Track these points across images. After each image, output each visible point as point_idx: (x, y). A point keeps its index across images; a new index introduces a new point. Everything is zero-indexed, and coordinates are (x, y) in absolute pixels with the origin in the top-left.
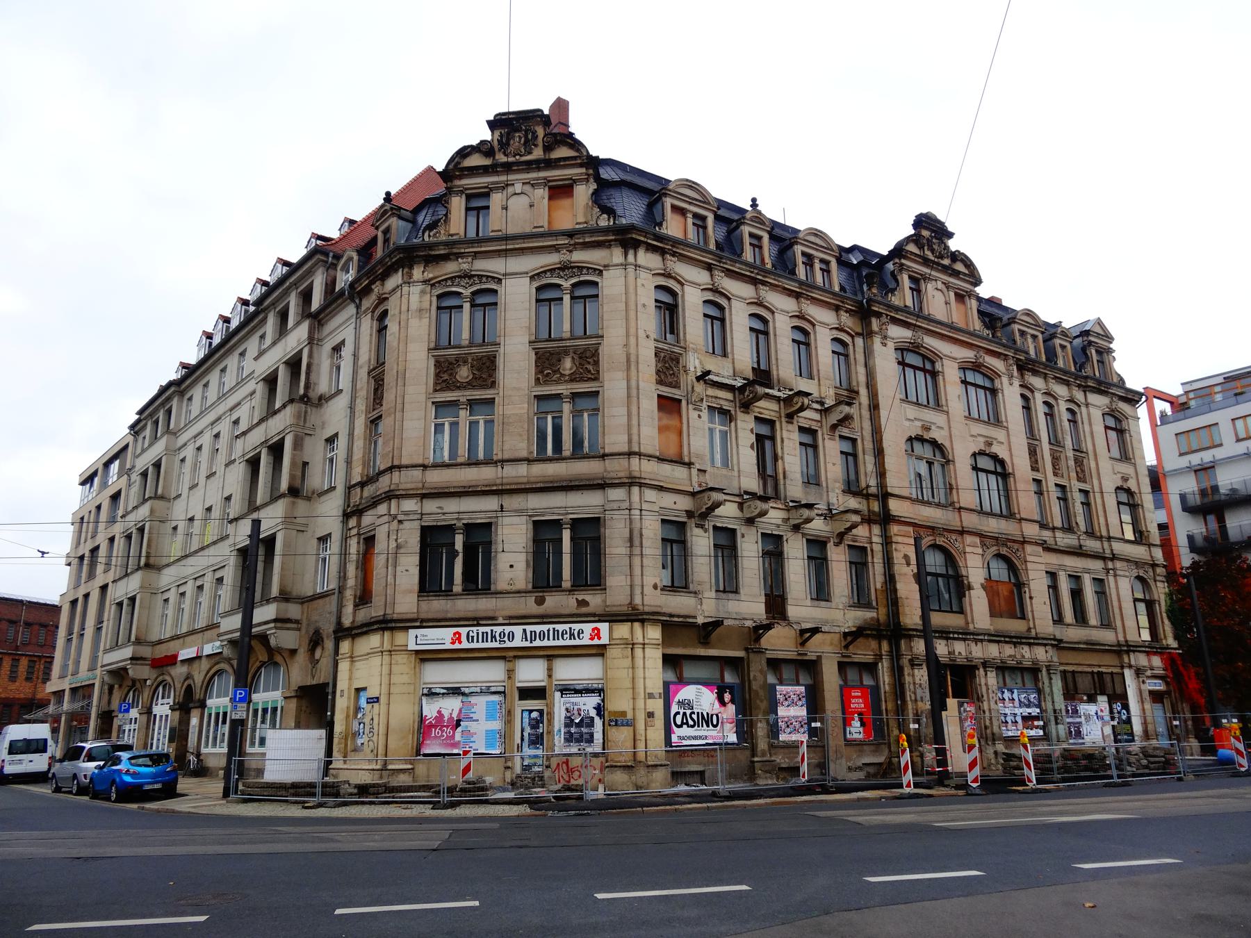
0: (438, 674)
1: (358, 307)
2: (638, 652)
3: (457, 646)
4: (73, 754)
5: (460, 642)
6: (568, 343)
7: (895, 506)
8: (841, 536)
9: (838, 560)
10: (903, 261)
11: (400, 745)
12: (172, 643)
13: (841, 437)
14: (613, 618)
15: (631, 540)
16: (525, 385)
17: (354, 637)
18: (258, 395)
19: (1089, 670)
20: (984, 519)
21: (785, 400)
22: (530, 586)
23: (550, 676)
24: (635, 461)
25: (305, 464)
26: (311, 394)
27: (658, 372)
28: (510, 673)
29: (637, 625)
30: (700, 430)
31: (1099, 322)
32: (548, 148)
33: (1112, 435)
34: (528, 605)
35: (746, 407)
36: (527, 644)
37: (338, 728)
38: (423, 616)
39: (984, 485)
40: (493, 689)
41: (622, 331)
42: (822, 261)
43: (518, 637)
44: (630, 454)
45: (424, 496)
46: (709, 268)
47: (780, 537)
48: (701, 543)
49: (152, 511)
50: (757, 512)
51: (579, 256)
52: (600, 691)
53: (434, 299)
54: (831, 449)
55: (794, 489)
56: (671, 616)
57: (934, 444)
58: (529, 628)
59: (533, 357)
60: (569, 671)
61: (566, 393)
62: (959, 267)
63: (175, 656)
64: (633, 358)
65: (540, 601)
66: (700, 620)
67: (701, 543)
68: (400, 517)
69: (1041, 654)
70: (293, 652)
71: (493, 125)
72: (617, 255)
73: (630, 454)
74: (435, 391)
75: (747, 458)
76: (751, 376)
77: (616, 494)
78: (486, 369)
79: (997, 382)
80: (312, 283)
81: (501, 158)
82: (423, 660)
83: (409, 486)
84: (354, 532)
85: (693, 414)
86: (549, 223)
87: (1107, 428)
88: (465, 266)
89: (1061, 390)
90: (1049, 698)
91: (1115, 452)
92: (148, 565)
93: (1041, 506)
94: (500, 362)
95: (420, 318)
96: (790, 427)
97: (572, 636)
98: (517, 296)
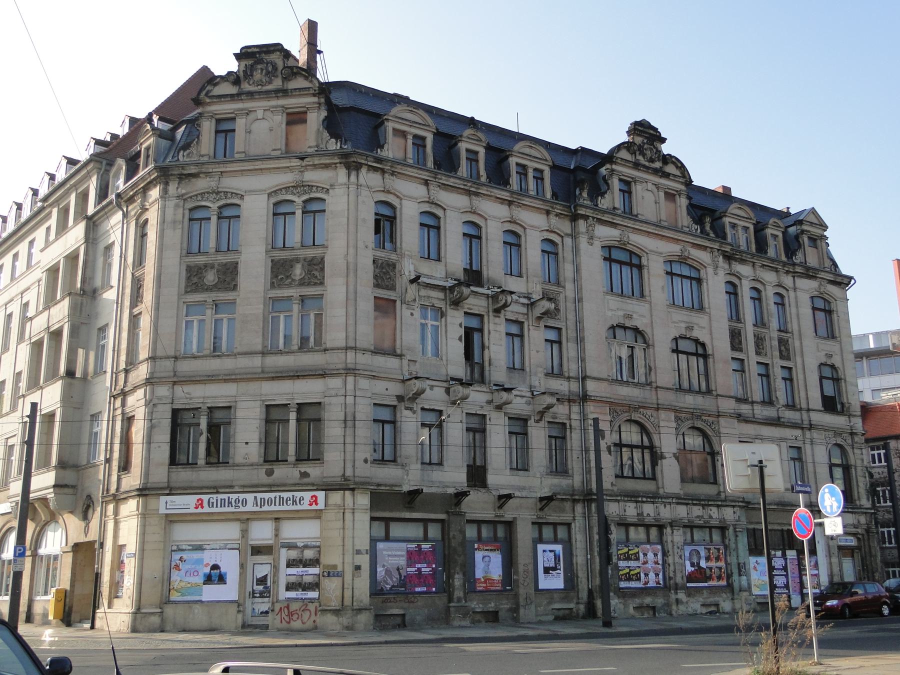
2: (348, 516)
3: (200, 510)
5: (202, 507)
7: (591, 386)
8: (542, 414)
9: (538, 435)
10: (614, 167)
13: (546, 326)
14: (328, 488)
16: (261, 288)
18: (43, 283)
19: (780, 528)
20: (680, 395)
21: (492, 297)
22: (262, 459)
23: (276, 535)
27: (375, 277)
28: (245, 533)
29: (347, 493)
30: (410, 325)
31: (813, 211)
32: (286, 79)
33: (821, 315)
35: (456, 304)
36: (258, 509)
39: (684, 366)
40: (229, 546)
41: (344, 243)
42: (535, 170)
43: (250, 502)
46: (426, 183)
47: (484, 416)
50: (460, 395)
51: (311, 176)
53: (187, 212)
54: (536, 336)
55: (498, 374)
56: (379, 485)
57: (636, 330)
58: (259, 496)
59: (270, 264)
60: (294, 531)
62: (670, 169)
64: (351, 267)
65: (270, 473)
66: (406, 488)
69: (729, 514)
71: (238, 57)
74: (186, 292)
75: (455, 349)
76: (461, 275)
77: (335, 383)
78: (229, 276)
79: (702, 272)
80: (89, 186)
81: (246, 87)
83: (163, 375)
85: (406, 313)
86: (287, 145)
87: (814, 309)
89: (770, 277)
90: (734, 553)
91: (822, 331)
93: (744, 384)
94: (241, 269)
95: (174, 229)
96: (497, 320)
97: (294, 502)
98: (255, 211)
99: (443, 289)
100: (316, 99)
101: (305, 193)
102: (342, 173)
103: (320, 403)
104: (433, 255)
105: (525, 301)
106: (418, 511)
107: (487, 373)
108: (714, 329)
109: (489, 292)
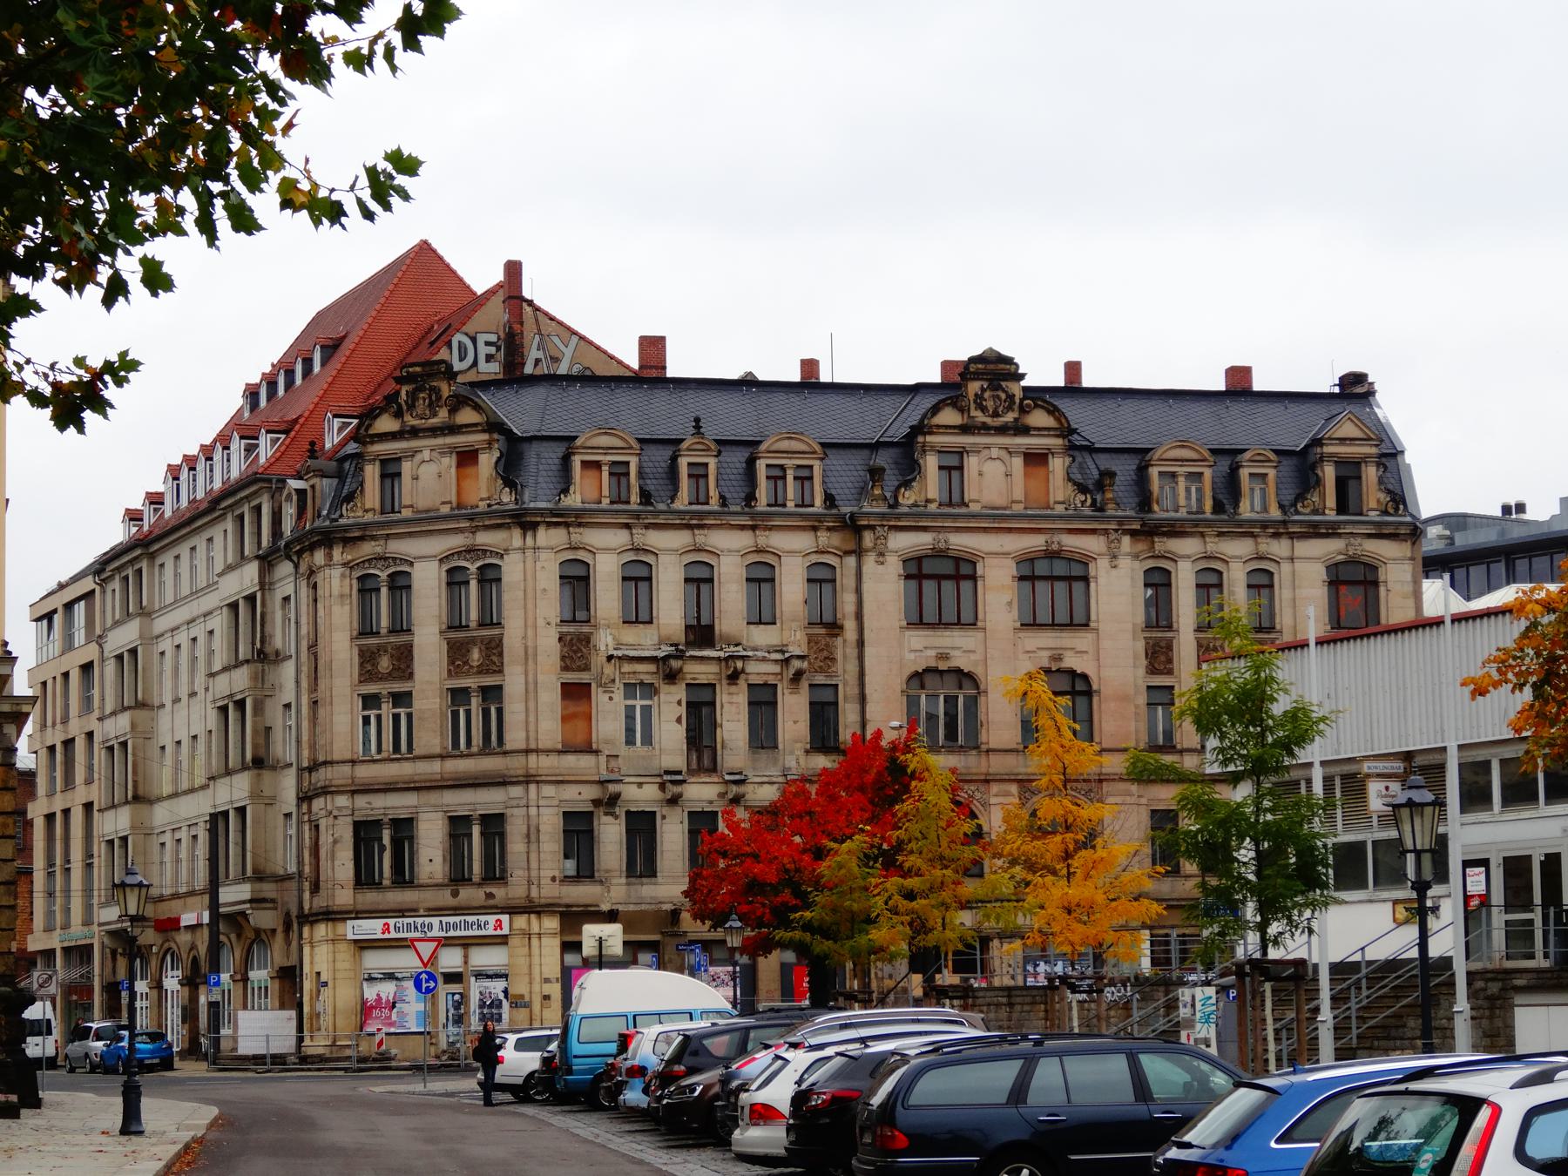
0: (376, 961)
1: (296, 566)
2: (535, 941)
3: (387, 936)
4: (78, 1033)
6: (475, 634)
11: (346, 1025)
12: (174, 903)
14: (512, 910)
15: (528, 836)
16: (436, 679)
17: (312, 923)
23: (466, 963)
24: (533, 758)
25: (268, 729)
26: (268, 649)
27: (563, 658)
32: (453, 411)
34: (444, 898)
35: (672, 677)
36: (443, 934)
37: (306, 1009)
38: (359, 907)
41: (521, 623)
44: (527, 751)
45: (353, 792)
48: (611, 835)
49: (133, 726)
51: (484, 538)
52: (506, 976)
53: (355, 582)
56: (568, 906)
58: (445, 919)
60: (485, 958)
61: (474, 686)
63: (178, 920)
64: (530, 651)
65: (455, 894)
67: (611, 835)
68: (335, 813)
70: (274, 931)
72: (516, 539)
73: (527, 751)
77: (516, 791)
82: (362, 948)
84: (306, 818)
86: (459, 493)
88: (379, 549)
92: (137, 798)
96: (733, 689)
98: (428, 581)
99: (653, 659)
100: (485, 436)
101: (479, 559)
102: (517, 533)
103: (502, 815)
104: (644, 616)
105: (778, 656)
106: (1490, 782)
107: (719, 759)
108: (1111, 649)
109: (721, 654)
